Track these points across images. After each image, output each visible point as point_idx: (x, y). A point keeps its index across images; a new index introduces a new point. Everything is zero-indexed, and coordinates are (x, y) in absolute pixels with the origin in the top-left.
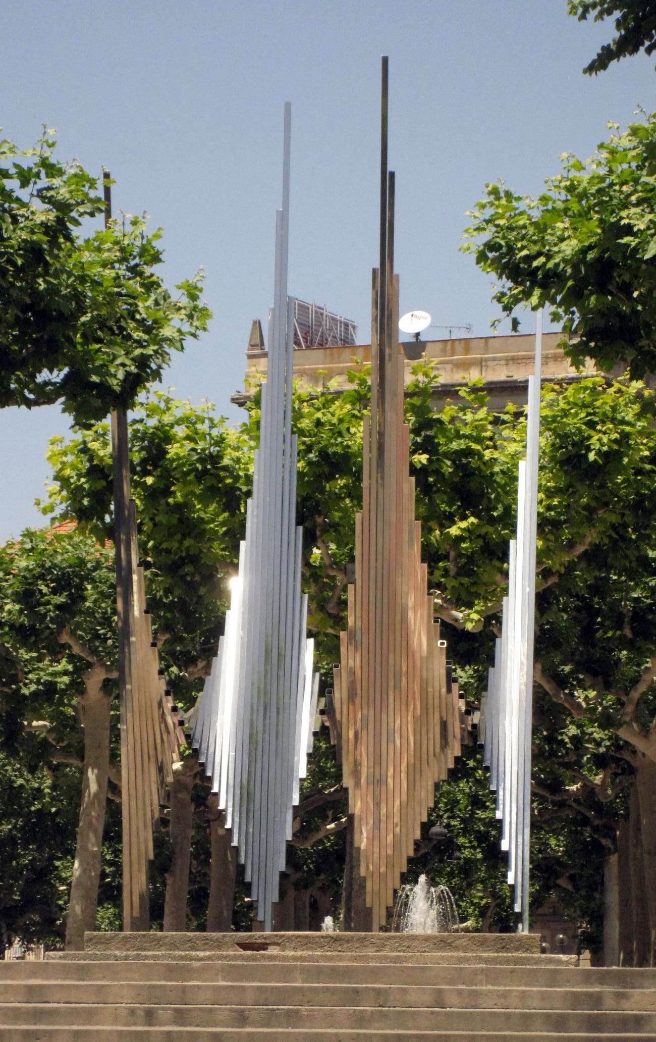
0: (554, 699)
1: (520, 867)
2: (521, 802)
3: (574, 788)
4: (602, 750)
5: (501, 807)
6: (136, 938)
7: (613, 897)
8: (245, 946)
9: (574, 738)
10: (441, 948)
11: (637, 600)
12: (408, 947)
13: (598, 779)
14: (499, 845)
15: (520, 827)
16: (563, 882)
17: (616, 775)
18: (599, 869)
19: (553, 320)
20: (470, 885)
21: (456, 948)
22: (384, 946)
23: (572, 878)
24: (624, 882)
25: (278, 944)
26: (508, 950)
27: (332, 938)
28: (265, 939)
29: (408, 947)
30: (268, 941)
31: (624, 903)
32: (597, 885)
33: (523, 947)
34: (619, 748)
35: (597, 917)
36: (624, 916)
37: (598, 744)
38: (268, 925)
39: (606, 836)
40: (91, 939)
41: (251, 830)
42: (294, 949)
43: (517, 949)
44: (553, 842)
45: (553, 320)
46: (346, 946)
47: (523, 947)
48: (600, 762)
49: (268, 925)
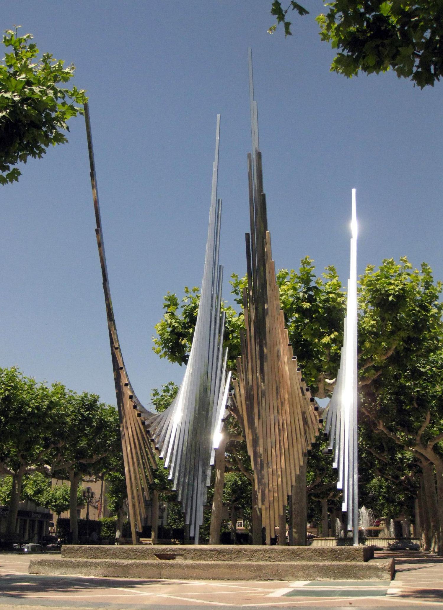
0: (389, 436)
1: (351, 501)
2: (351, 458)
3: (403, 478)
4: (410, 462)
5: (336, 460)
6: (92, 550)
7: (417, 511)
8: (161, 556)
9: (400, 458)
10: (292, 558)
11: (418, 391)
12: (269, 557)
13: (410, 475)
14: (336, 486)
15: (351, 473)
16: (405, 507)
17: (416, 473)
18: (413, 503)
19: (323, 40)
20: (384, 508)
21: (303, 558)
22: (253, 556)
23: (407, 506)
24: (420, 507)
25: (182, 555)
26: (340, 559)
27: (218, 551)
28: (174, 551)
29: (269, 557)
30: (175, 553)
31: (420, 513)
32: (412, 508)
33: (351, 557)
34: (416, 461)
35: (414, 516)
36: (421, 516)
37: (408, 460)
38: (197, 540)
39: (415, 494)
40: (65, 550)
41: (187, 481)
42: (193, 559)
43: (346, 559)
44: (401, 497)
45: (323, 40)
46: (227, 556)
47: (351, 557)
48: (410, 467)
49: (197, 540)
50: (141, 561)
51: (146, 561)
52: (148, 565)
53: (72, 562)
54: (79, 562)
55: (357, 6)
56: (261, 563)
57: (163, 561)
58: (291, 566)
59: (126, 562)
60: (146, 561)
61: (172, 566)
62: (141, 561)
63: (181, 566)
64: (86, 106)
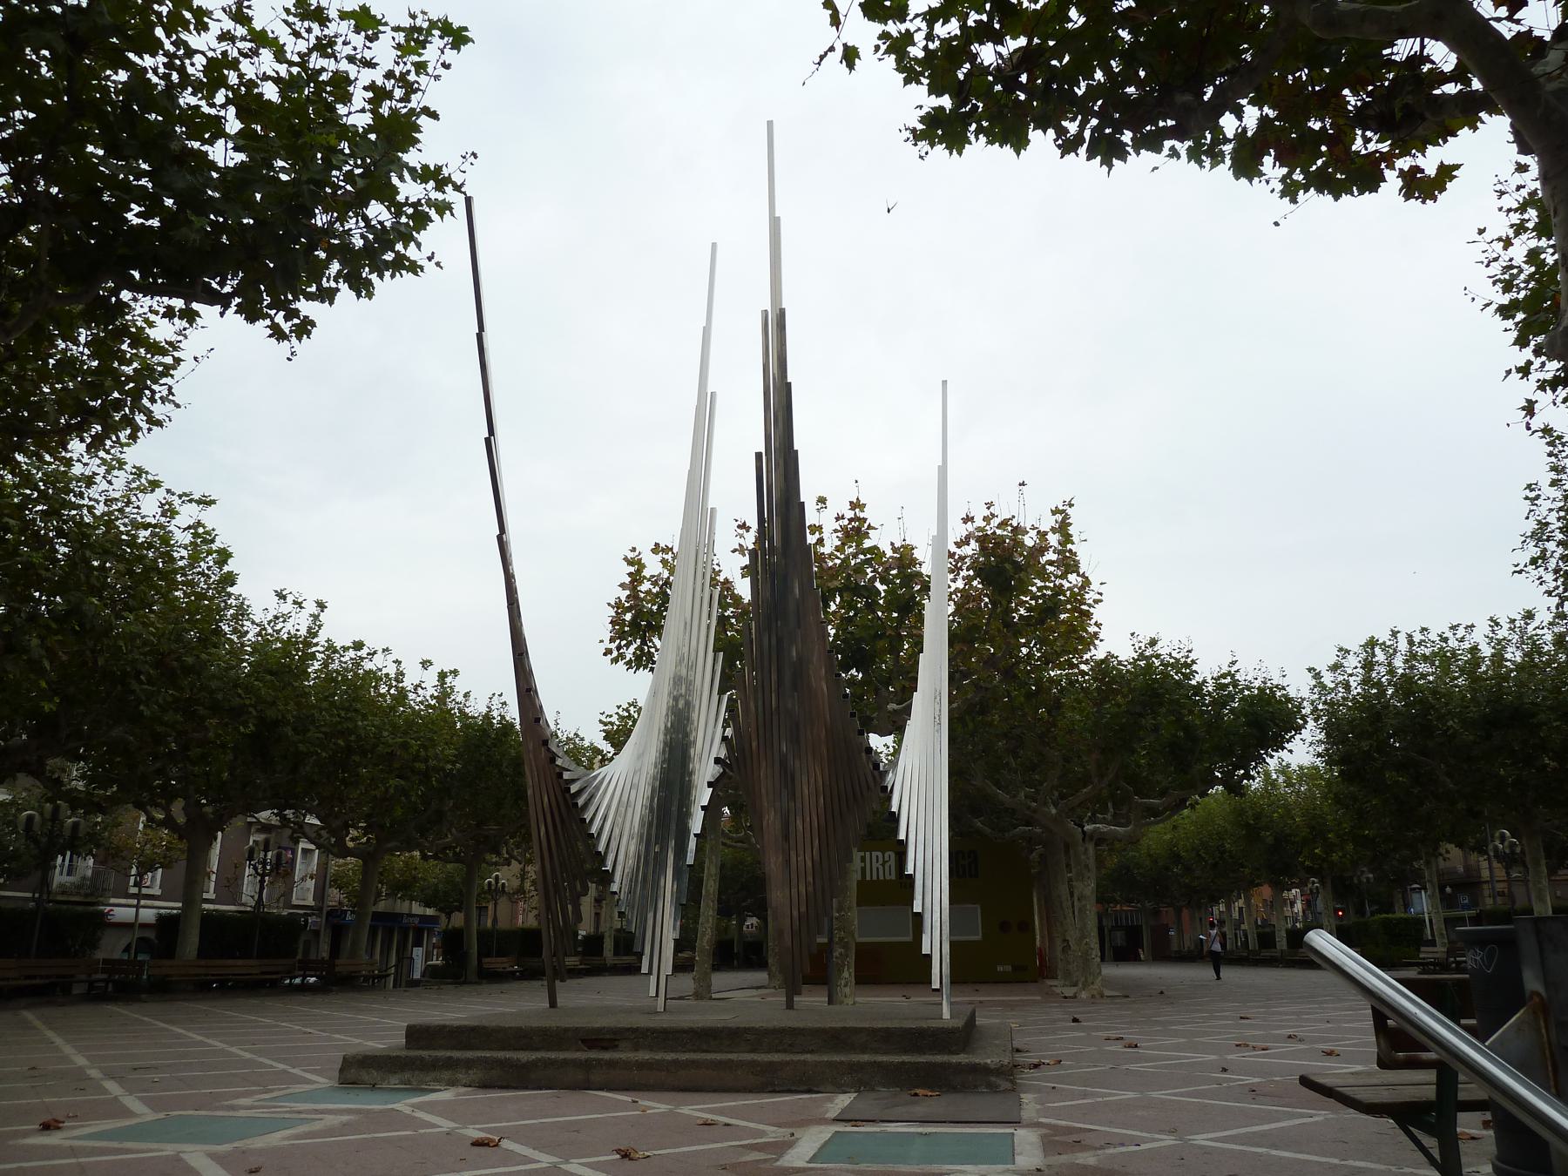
26: (921, 1051)
50: (553, 1055)
51: (562, 1055)
52: (565, 1062)
53: (422, 1059)
54: (437, 1059)
55: (1493, 110)
56: (776, 1057)
57: (593, 1055)
58: (830, 1064)
59: (524, 1056)
60: (562, 1055)
61: (611, 1064)
62: (553, 1055)
63: (627, 1065)
64: (468, 200)
